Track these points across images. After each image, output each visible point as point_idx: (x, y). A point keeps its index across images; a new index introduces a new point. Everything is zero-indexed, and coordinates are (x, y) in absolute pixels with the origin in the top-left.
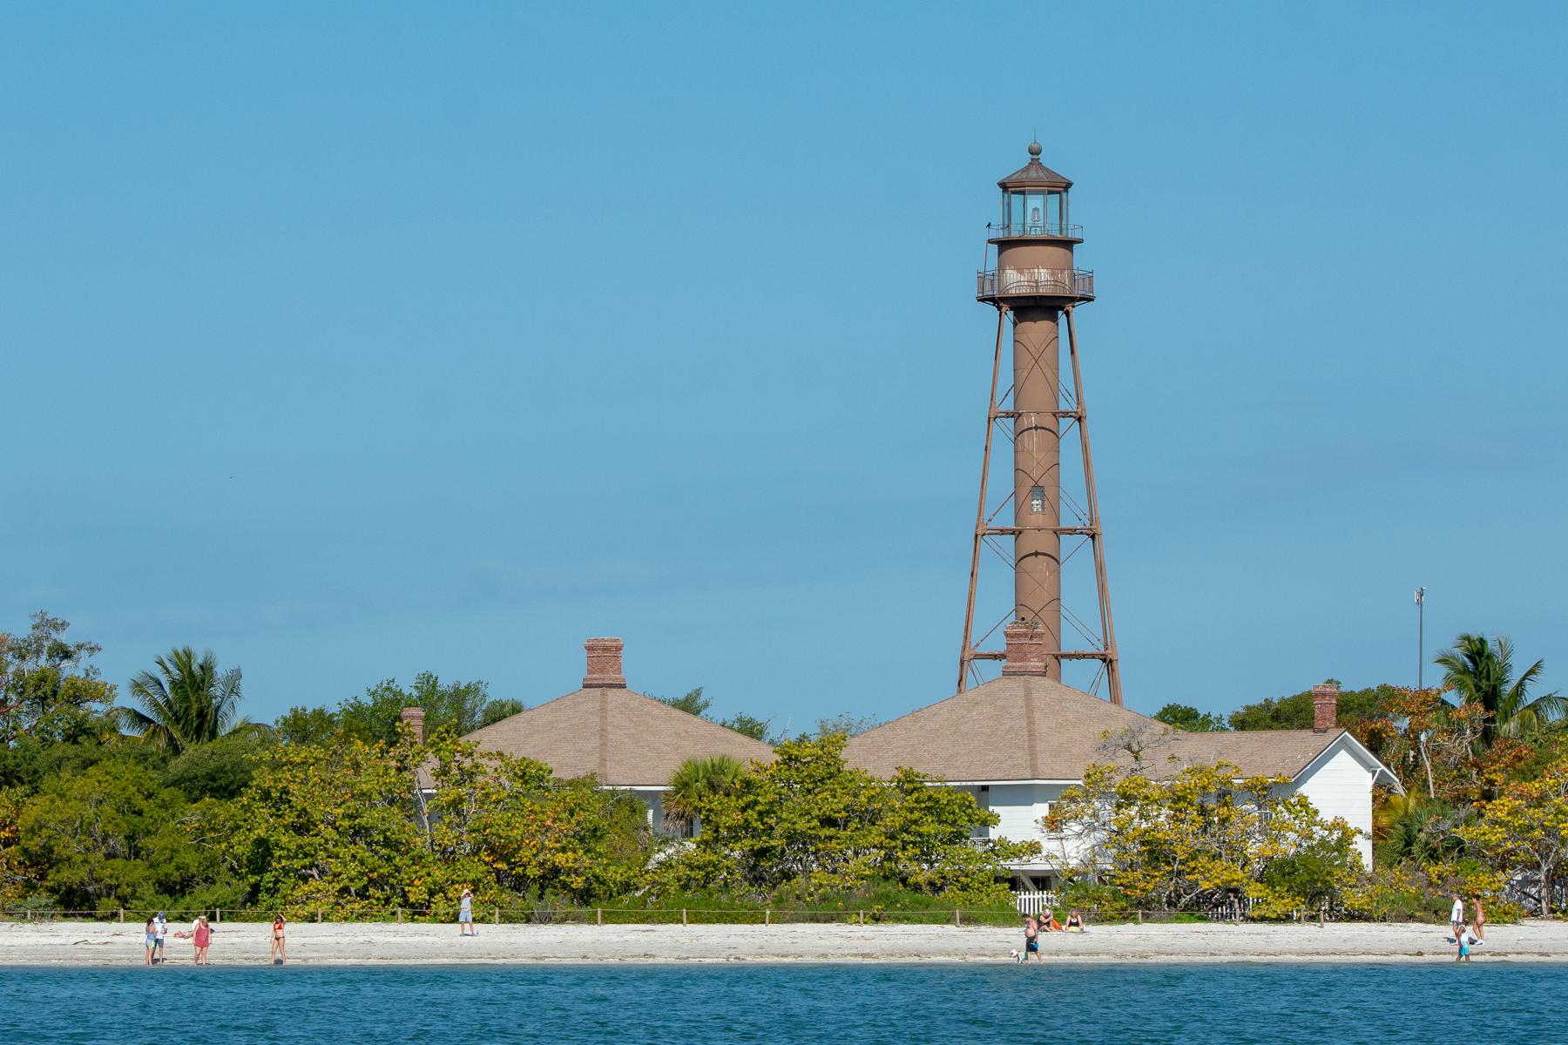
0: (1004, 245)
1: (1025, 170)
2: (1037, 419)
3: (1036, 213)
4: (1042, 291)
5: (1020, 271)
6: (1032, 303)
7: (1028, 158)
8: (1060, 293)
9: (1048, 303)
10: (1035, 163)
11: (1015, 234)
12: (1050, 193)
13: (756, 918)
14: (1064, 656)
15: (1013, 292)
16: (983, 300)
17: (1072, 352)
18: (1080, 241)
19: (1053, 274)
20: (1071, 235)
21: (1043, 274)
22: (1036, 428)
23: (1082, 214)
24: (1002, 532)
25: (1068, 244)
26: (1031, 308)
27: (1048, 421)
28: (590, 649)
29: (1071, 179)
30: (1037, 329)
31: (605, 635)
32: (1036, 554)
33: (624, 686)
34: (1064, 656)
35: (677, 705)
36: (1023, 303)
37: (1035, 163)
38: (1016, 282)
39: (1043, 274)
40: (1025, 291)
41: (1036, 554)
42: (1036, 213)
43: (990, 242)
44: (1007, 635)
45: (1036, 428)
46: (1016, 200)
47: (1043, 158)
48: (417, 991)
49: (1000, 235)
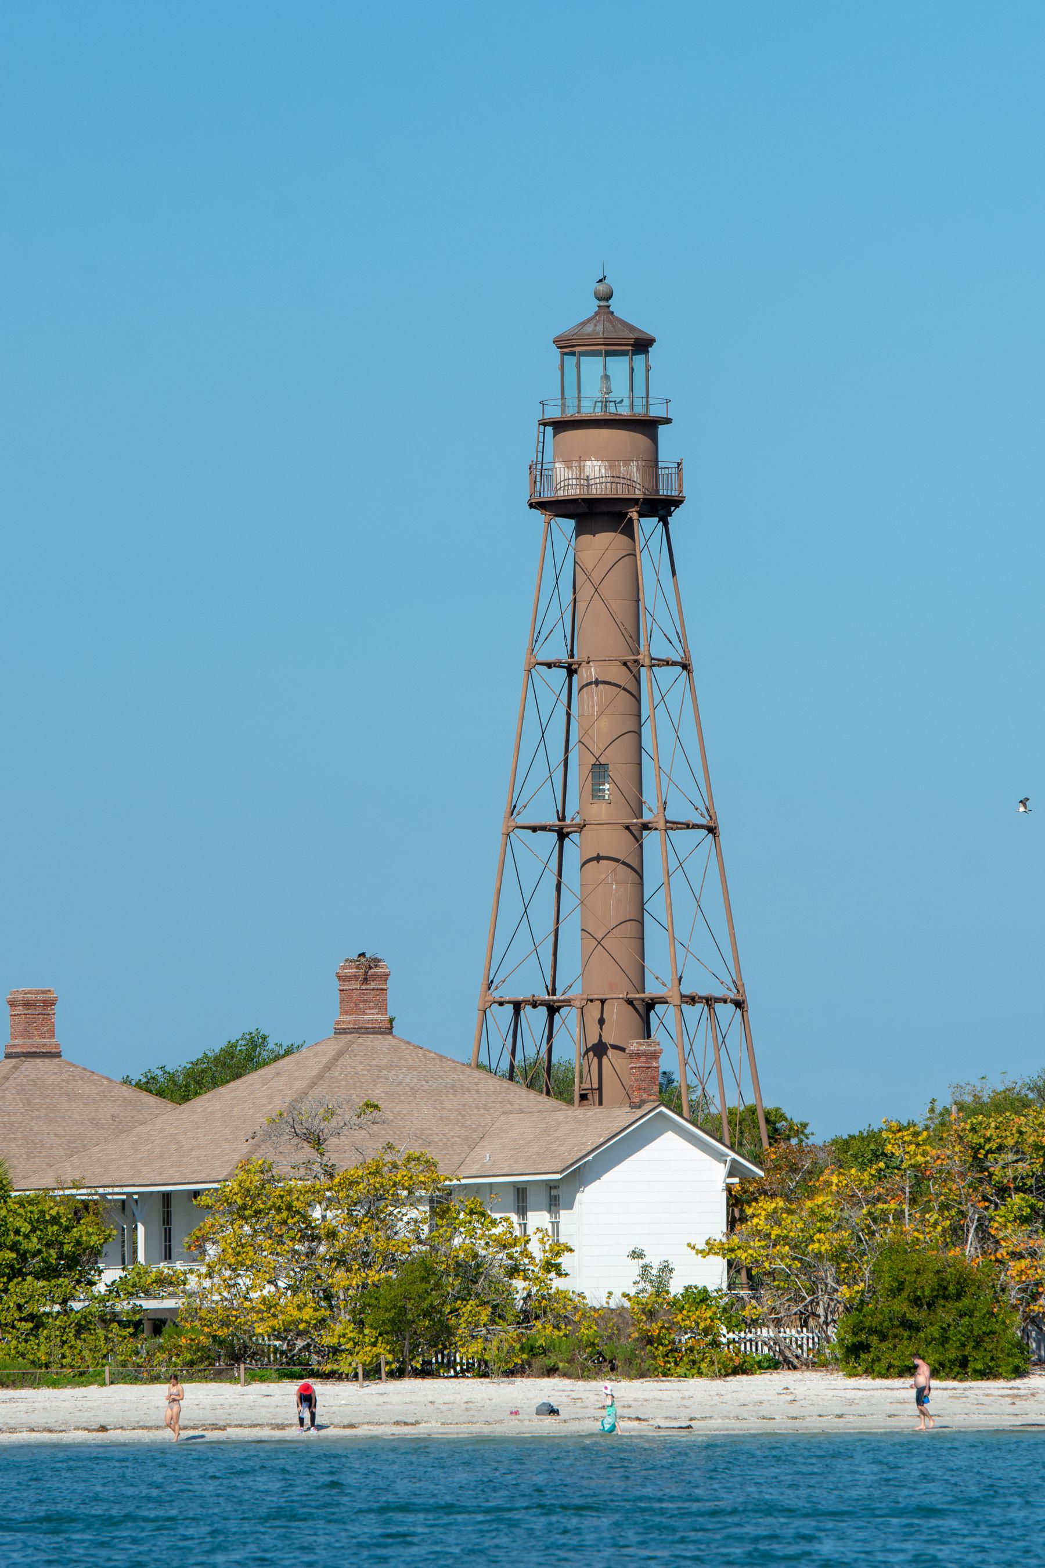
0: (560, 426)
1: (584, 324)
2: (618, 671)
3: (604, 383)
4: (595, 492)
7: (594, 305)
8: (622, 493)
10: (605, 311)
11: (571, 413)
12: (608, 354)
13: (82, 1377)
15: (562, 494)
17: (674, 573)
18: (667, 421)
21: (595, 468)
22: (597, 683)
23: (667, 382)
25: (647, 426)
26: (591, 513)
27: (621, 675)
28: (12, 1004)
29: (647, 327)
30: (604, 543)
31: (29, 985)
32: (598, 858)
33: (57, 1055)
37: (605, 311)
38: (564, 482)
39: (595, 468)
40: (573, 493)
41: (598, 858)
42: (604, 383)
45: (597, 683)
46: (570, 361)
48: (120, 1449)
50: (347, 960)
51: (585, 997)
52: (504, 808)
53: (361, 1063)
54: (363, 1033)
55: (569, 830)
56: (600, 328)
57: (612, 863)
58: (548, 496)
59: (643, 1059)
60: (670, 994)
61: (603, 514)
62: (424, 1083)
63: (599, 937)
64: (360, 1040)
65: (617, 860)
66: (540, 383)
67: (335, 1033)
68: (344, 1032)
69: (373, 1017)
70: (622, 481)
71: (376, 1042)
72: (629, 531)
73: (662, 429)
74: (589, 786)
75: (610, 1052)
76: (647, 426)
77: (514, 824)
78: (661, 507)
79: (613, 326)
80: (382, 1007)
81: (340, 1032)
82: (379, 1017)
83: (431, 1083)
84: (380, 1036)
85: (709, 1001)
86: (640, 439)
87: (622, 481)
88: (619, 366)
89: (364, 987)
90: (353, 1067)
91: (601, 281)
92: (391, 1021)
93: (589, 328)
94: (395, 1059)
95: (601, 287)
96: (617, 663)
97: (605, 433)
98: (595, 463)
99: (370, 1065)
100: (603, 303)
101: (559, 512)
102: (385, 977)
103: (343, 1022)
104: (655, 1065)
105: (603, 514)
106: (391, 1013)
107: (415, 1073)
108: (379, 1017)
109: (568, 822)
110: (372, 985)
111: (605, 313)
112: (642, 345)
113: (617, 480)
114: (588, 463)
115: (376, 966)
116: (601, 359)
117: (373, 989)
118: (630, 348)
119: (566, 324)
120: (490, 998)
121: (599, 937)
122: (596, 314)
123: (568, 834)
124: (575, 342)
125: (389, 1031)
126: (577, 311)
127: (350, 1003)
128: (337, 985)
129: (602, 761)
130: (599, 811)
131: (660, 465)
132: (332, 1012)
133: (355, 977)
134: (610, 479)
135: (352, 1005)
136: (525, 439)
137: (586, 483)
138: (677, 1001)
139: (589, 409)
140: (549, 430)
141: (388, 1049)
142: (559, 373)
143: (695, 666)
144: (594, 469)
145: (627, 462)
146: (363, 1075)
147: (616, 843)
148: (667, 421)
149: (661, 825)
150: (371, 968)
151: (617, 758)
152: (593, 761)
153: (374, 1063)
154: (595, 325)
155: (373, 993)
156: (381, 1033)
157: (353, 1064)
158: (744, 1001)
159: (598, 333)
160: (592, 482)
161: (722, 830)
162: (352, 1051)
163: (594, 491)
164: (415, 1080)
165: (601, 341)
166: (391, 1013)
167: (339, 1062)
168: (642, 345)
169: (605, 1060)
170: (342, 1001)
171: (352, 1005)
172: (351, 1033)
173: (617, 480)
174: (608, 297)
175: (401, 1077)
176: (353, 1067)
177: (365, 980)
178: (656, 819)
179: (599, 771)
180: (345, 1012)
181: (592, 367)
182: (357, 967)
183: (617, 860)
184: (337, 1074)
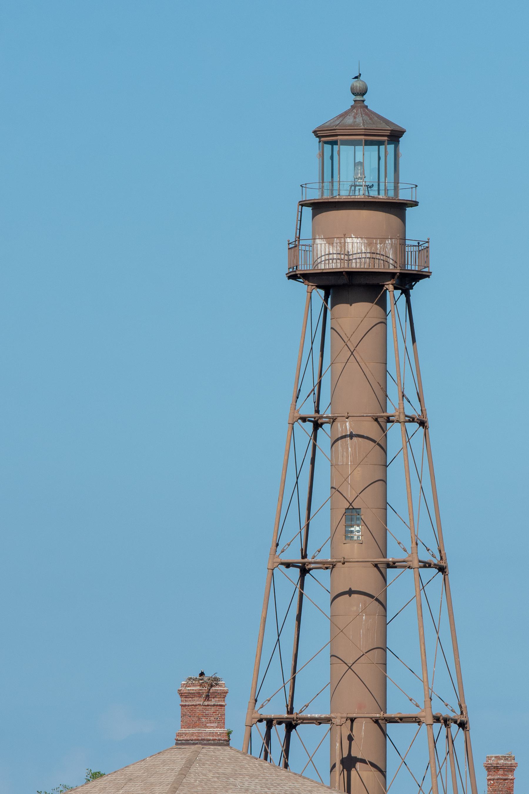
0: (319, 207)
1: (344, 115)
2: (363, 428)
3: (357, 169)
4: (355, 266)
5: (330, 240)
6: (344, 280)
7: (350, 100)
8: (379, 267)
9: (363, 281)
10: (359, 105)
11: (327, 197)
14: (392, 720)
15: (323, 267)
16: (293, 277)
18: (415, 204)
19: (369, 244)
20: (404, 195)
21: (355, 245)
22: (351, 436)
23: (417, 170)
24: (288, 565)
25: (397, 208)
26: (341, 286)
27: (370, 428)
29: (400, 122)
30: (356, 314)
32: (350, 592)
34: (392, 720)
35: (86, 784)
36: (332, 281)
37: (359, 105)
38: (325, 256)
39: (355, 245)
41: (350, 592)
42: (357, 169)
43: (303, 204)
44: (181, 695)
45: (351, 436)
47: (369, 100)
49: (314, 195)
50: (190, 679)
51: (345, 715)
52: (271, 544)
53: (210, 771)
54: (205, 744)
55: (312, 566)
56: (359, 120)
57: (363, 596)
58: (304, 267)
59: (501, 772)
60: (423, 714)
61: (360, 286)
62: (267, 790)
63: (350, 662)
64: (204, 751)
65: (372, 596)
66: (302, 170)
67: (177, 744)
68: (187, 743)
69: (212, 730)
70: (378, 256)
71: (218, 753)
72: (382, 304)
73: (409, 211)
74: (342, 528)
75: (358, 765)
76: (397, 208)
77: (279, 561)
78: (407, 281)
79: (371, 119)
80: (221, 722)
81: (181, 743)
82: (219, 730)
83: (272, 790)
84: (219, 747)
85: (446, 722)
86: (393, 219)
87: (378, 256)
88: (369, 155)
89: (206, 703)
90: (205, 775)
91: (356, 78)
92: (229, 733)
93: (349, 120)
94: (237, 768)
95: (358, 84)
96: (370, 419)
97: (365, 213)
98: (355, 240)
99: (218, 773)
100: (359, 98)
101: (322, 283)
102: (223, 694)
103: (186, 734)
104: (510, 777)
105: (360, 286)
106: (228, 726)
107: (257, 781)
108: (219, 730)
109: (309, 559)
110: (213, 702)
111: (361, 107)
112: (395, 136)
113: (374, 256)
114: (349, 240)
115: (217, 684)
116: (376, 147)
117: (214, 705)
118: (386, 138)
119: (325, 117)
120: (257, 716)
121: (350, 662)
122: (353, 107)
123: (310, 569)
124: (338, 132)
125: (227, 742)
126: (337, 104)
127: (190, 717)
128: (178, 700)
129: (355, 505)
130: (351, 551)
131: (408, 242)
132: (173, 724)
133: (199, 694)
134: (368, 255)
135: (195, 719)
136: (284, 218)
137: (346, 257)
138: (430, 720)
139: (344, 193)
140: (308, 211)
141: (230, 759)
142: (330, 161)
143: (430, 423)
144: (352, 247)
145: (383, 240)
146: (215, 782)
147: (363, 578)
148: (415, 204)
149: (416, 564)
150: (212, 686)
151: (367, 503)
152: (347, 505)
153: (221, 771)
154: (355, 118)
155: (213, 709)
156: (220, 745)
157: (204, 772)
158: (467, 722)
159: (358, 125)
160: (351, 257)
161: (450, 570)
162: (200, 760)
163: (354, 265)
164: (258, 787)
165: (362, 132)
166: (228, 726)
167: (192, 770)
168: (395, 136)
169: (353, 772)
170: (183, 715)
171: (195, 719)
172: (194, 744)
173: (374, 256)
174: (363, 93)
175: (246, 784)
176: (205, 775)
177: (208, 697)
178: (410, 559)
179: (352, 514)
180: (186, 725)
181: (347, 155)
182: (201, 685)
183: (372, 596)
184: (192, 781)
